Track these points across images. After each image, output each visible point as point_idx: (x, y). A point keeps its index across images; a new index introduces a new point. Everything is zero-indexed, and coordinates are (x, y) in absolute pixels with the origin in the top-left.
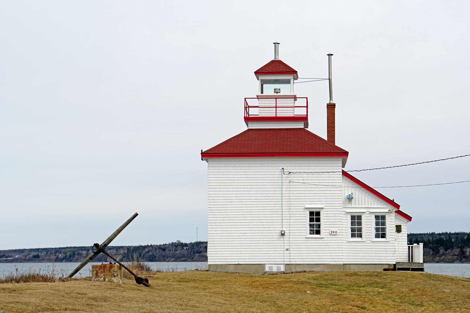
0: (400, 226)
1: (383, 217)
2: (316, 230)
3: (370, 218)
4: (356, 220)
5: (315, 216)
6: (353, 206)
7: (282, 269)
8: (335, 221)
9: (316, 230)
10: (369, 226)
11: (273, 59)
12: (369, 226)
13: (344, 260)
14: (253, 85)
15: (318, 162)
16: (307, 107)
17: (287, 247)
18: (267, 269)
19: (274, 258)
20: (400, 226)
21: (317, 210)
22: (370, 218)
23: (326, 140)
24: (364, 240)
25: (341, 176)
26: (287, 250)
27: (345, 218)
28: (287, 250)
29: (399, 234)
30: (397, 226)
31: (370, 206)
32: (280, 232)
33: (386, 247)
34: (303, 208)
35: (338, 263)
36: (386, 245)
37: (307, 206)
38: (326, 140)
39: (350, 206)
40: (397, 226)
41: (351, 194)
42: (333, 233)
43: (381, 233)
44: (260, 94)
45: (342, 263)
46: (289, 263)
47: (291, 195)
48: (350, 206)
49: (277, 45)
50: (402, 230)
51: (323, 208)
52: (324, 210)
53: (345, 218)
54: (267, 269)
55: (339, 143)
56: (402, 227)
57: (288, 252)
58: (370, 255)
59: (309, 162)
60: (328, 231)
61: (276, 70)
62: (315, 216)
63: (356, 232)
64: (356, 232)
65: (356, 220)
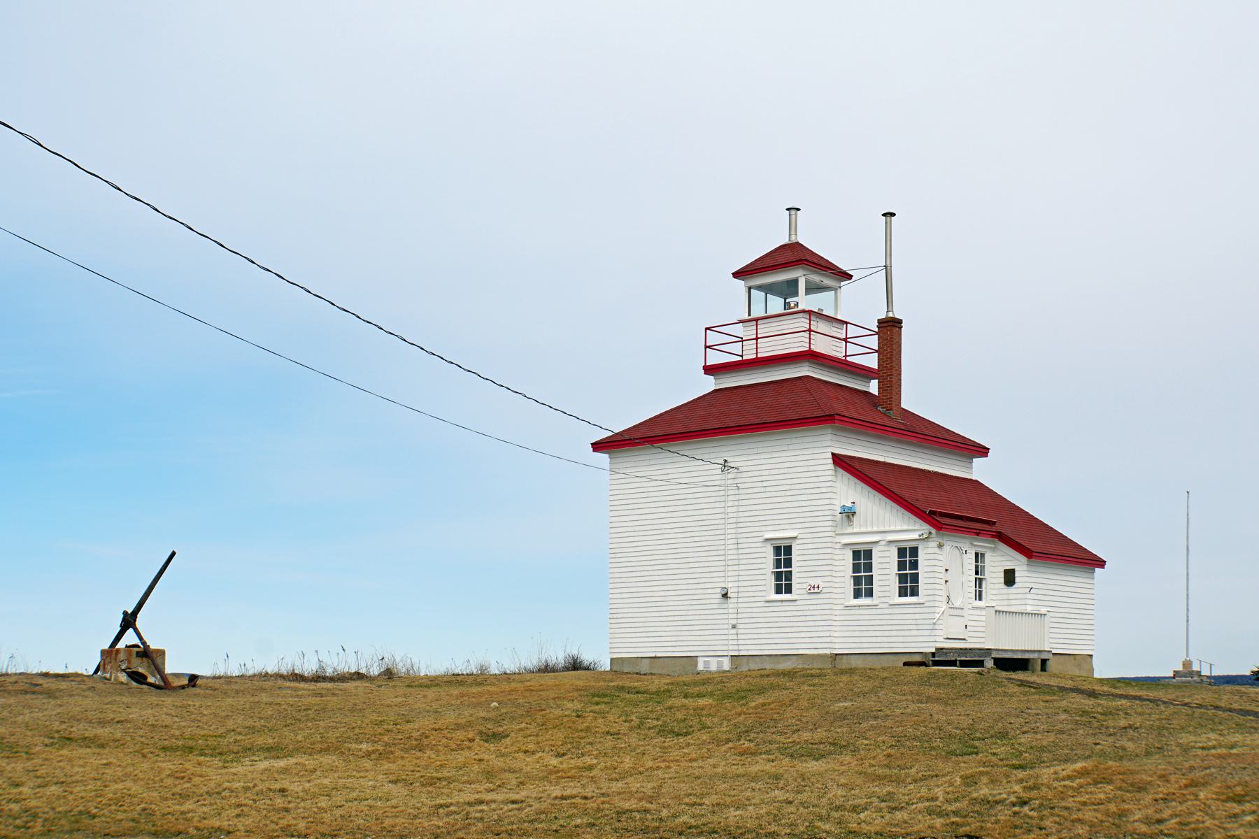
0: (1013, 571)
1: (914, 551)
2: (783, 583)
3: (887, 554)
4: (862, 559)
5: (783, 554)
6: (856, 530)
7: (726, 665)
8: (825, 567)
9: (783, 583)
10: (885, 569)
11: (785, 241)
12: (885, 569)
13: (837, 646)
14: (735, 299)
15: (788, 441)
16: (706, 347)
17: (734, 622)
18: (701, 667)
19: (711, 642)
20: (1013, 571)
21: (867, 547)
22: (887, 554)
23: (876, 393)
24: (876, 602)
25: (832, 466)
26: (734, 627)
27: (841, 557)
28: (734, 627)
29: (1012, 590)
30: (1006, 572)
31: (887, 528)
32: (719, 590)
33: (917, 616)
34: (761, 539)
35: (821, 652)
36: (917, 610)
37: (768, 536)
38: (876, 393)
39: (850, 530)
40: (1006, 572)
41: (849, 505)
42: (814, 590)
43: (909, 584)
44: (746, 317)
45: (828, 652)
46: (736, 653)
47: (741, 514)
48: (850, 530)
49: (793, 212)
50: (1002, 575)
51: (795, 538)
52: (798, 542)
53: (841, 557)
54: (701, 667)
55: (911, 400)
56: (1017, 574)
57: (734, 631)
58: (886, 633)
59: (772, 443)
60: (805, 586)
61: (788, 266)
62: (783, 554)
63: (863, 586)
64: (863, 586)
65: (862, 559)
